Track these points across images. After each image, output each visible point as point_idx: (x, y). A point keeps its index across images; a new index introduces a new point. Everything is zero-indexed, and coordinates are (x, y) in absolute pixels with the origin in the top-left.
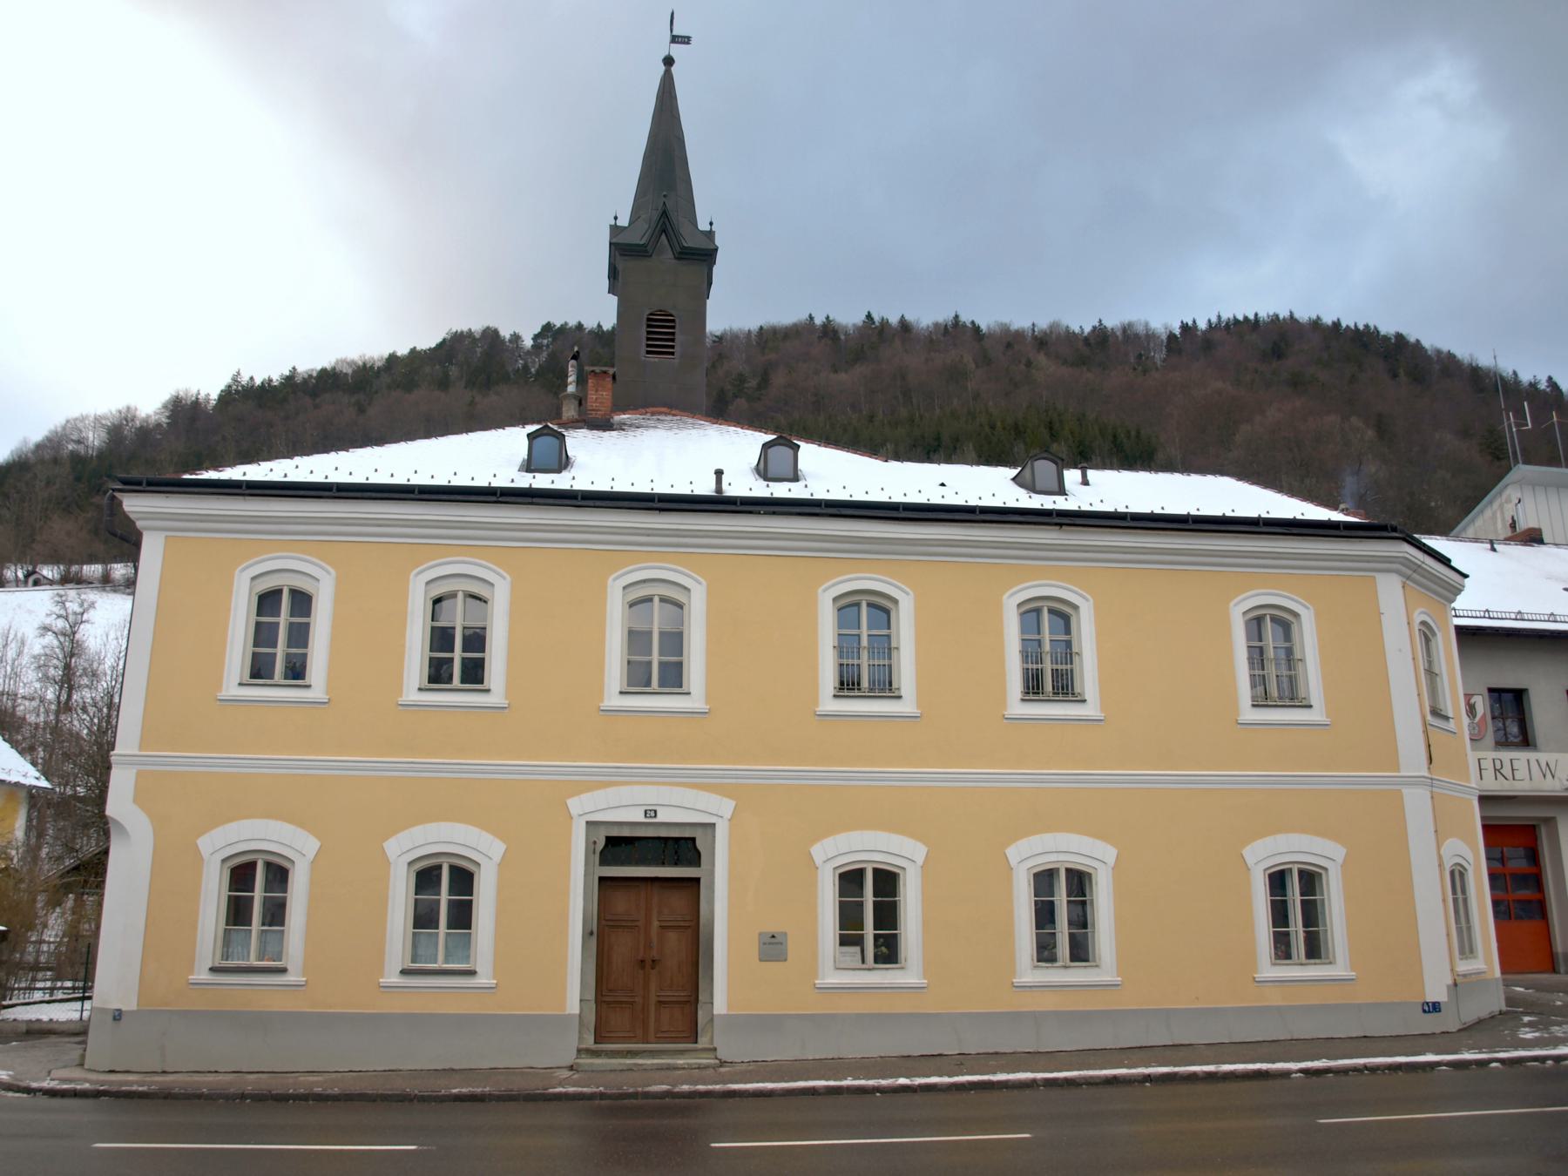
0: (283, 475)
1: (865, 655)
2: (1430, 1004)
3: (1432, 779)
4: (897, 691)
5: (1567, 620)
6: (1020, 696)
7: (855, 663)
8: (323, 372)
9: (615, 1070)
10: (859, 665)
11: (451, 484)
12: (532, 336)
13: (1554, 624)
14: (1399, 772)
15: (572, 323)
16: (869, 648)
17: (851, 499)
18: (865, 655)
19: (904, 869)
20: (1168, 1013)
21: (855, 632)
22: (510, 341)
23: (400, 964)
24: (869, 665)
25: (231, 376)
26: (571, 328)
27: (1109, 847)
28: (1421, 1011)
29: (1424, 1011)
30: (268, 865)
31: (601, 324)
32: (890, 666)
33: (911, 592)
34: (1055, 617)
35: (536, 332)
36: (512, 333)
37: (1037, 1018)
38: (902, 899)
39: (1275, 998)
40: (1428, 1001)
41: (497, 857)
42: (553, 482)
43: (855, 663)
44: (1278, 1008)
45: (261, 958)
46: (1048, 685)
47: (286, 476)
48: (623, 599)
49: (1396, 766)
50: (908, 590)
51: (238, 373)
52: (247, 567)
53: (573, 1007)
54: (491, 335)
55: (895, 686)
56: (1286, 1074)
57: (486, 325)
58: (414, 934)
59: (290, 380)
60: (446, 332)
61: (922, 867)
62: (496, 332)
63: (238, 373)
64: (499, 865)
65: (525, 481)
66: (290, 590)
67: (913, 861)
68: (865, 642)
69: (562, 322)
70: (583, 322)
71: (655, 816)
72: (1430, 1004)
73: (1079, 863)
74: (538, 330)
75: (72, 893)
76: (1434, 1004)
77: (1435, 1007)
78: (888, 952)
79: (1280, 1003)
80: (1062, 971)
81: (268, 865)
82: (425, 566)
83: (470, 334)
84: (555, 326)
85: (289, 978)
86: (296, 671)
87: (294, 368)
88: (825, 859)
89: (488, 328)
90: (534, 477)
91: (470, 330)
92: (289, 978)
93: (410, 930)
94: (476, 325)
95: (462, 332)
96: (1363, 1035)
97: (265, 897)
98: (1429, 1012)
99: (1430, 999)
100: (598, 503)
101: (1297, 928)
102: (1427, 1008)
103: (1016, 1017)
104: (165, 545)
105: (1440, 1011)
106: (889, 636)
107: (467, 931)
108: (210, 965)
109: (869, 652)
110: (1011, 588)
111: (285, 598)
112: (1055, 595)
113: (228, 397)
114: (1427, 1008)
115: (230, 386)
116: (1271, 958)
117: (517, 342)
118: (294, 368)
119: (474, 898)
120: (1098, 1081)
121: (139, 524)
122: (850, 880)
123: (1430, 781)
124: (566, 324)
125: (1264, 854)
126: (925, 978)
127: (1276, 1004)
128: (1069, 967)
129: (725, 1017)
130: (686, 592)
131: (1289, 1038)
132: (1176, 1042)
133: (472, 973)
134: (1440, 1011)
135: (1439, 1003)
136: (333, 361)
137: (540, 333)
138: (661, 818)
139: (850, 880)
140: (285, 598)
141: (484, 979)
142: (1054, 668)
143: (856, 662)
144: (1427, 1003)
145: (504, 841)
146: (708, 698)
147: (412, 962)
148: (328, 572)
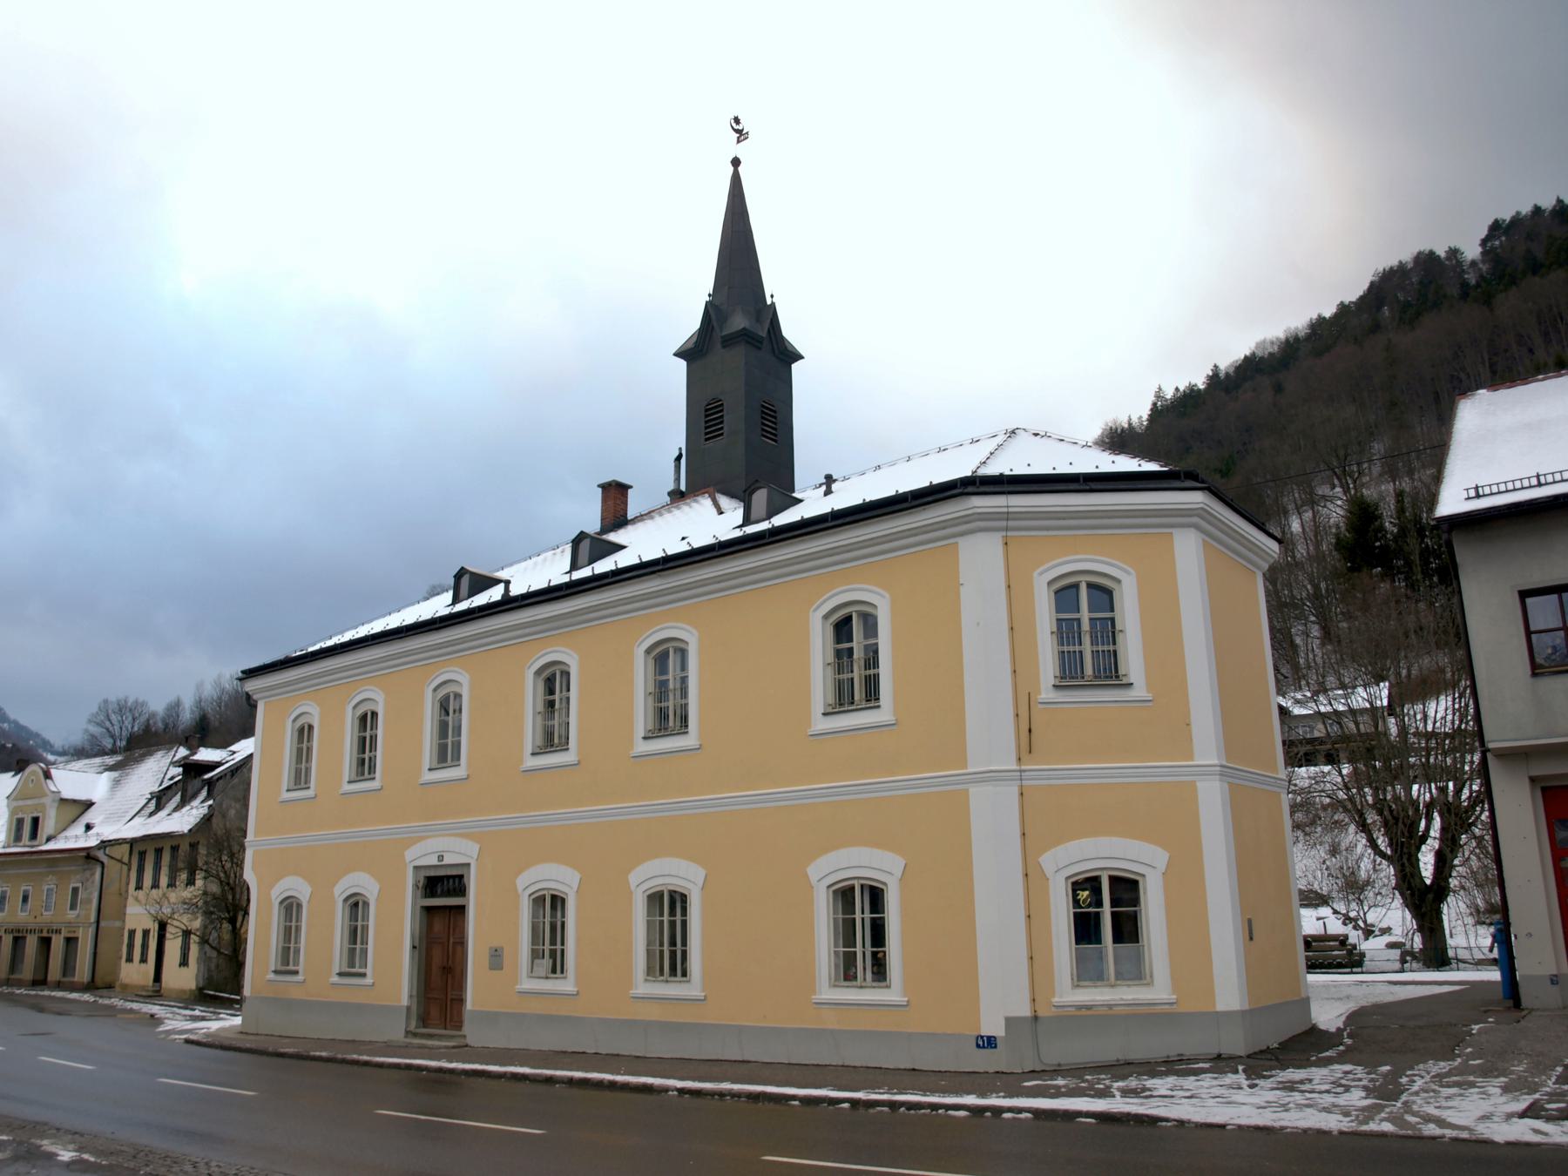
1: (1086, 640)
2: (985, 1038)
3: (1021, 771)
4: (1124, 678)
5: (1567, 475)
6: (1052, 681)
7: (1100, 649)
8: (1246, 358)
10: (1081, 652)
12: (1479, 242)
13: (1538, 489)
14: (966, 768)
15: (1526, 209)
16: (1091, 633)
18: (1086, 640)
19: (1143, 876)
20: (740, 1030)
22: (1448, 258)
24: (1093, 652)
25: (1153, 394)
26: (1526, 216)
27: (700, 869)
28: (975, 1044)
29: (978, 1046)
31: (1561, 198)
32: (1115, 652)
33: (1133, 572)
34: (1094, 591)
35: (1483, 237)
36: (1447, 249)
37: (646, 1026)
39: (831, 1021)
40: (983, 1034)
43: (1100, 649)
44: (832, 1032)
49: (959, 755)
50: (1130, 569)
51: (1160, 389)
53: (405, 1001)
54: (1427, 261)
55: (1121, 672)
56: (666, 1090)
57: (1415, 251)
59: (1216, 380)
60: (1372, 273)
62: (1432, 253)
63: (1160, 389)
64: (901, 880)
67: (1154, 867)
68: (1086, 626)
69: (1513, 213)
70: (1539, 204)
71: (442, 860)
72: (985, 1038)
73: (1126, 867)
74: (1484, 233)
76: (989, 1038)
77: (990, 1042)
78: (557, 966)
79: (837, 1027)
80: (663, 985)
83: (1401, 265)
84: (1504, 221)
85: (300, 978)
87: (1216, 366)
88: (1056, 869)
89: (1420, 253)
91: (1400, 262)
94: (1401, 252)
95: (1391, 268)
96: (911, 1067)
98: (984, 1047)
99: (985, 1032)
101: (862, 948)
102: (981, 1043)
103: (631, 1024)
104: (265, 710)
105: (996, 1047)
106: (1113, 620)
109: (1091, 637)
110: (1039, 567)
112: (1057, 575)
113: (1156, 412)
114: (981, 1043)
115: (1155, 404)
116: (1072, 979)
117: (1456, 257)
118: (1216, 366)
119: (886, 915)
120: (541, 1079)
121: (255, 697)
122: (844, 895)
123: (1019, 774)
124: (1518, 213)
125: (342, 888)
127: (830, 1027)
128: (550, 978)
129: (472, 1012)
131: (840, 1063)
132: (746, 1058)
134: (996, 1047)
135: (994, 1037)
136: (1253, 346)
137: (1487, 236)
138: (447, 861)
139: (844, 895)
142: (1094, 649)
143: (1077, 648)
144: (982, 1037)
146: (1150, 686)
147: (349, 967)
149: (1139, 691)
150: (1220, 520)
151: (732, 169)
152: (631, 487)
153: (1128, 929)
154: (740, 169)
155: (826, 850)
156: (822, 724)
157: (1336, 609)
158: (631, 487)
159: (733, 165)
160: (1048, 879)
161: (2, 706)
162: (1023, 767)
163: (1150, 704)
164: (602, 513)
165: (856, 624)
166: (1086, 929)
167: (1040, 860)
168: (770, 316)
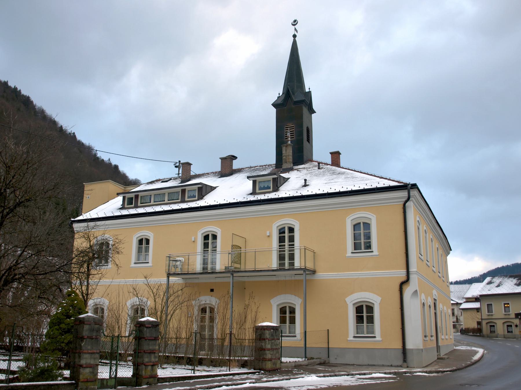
0: (383, 184)
9: (354, 365)
11: (156, 211)
17: (384, 186)
21: (359, 232)
23: (353, 335)
30: (367, 306)
38: (374, 314)
41: (379, 302)
42: (347, 188)
45: (290, 333)
46: (204, 258)
47: (290, 195)
48: (351, 223)
52: (350, 217)
58: (357, 326)
61: (379, 304)
65: (252, 198)
66: (212, 234)
75: (519, 316)
81: (367, 306)
82: (277, 222)
86: (368, 246)
90: (279, 196)
92: (377, 339)
93: (356, 324)
97: (290, 316)
100: (301, 199)
107: (285, 324)
108: (353, 336)
111: (362, 225)
126: (381, 338)
130: (370, 220)
133: (375, 337)
140: (362, 225)
141: (378, 338)
145: (381, 297)
148: (374, 216)
149: (376, 252)
150: (419, 202)
151: (293, 38)
152: (192, 164)
153: (371, 320)
154: (296, 39)
155: (365, 291)
156: (133, 265)
157: (91, 267)
158: (192, 164)
159: (293, 37)
160: (347, 304)
161: (3, 79)
162: (137, 280)
163: (378, 256)
164: (83, 201)
165: (144, 242)
166: (359, 319)
167: (346, 299)
168: (310, 96)
